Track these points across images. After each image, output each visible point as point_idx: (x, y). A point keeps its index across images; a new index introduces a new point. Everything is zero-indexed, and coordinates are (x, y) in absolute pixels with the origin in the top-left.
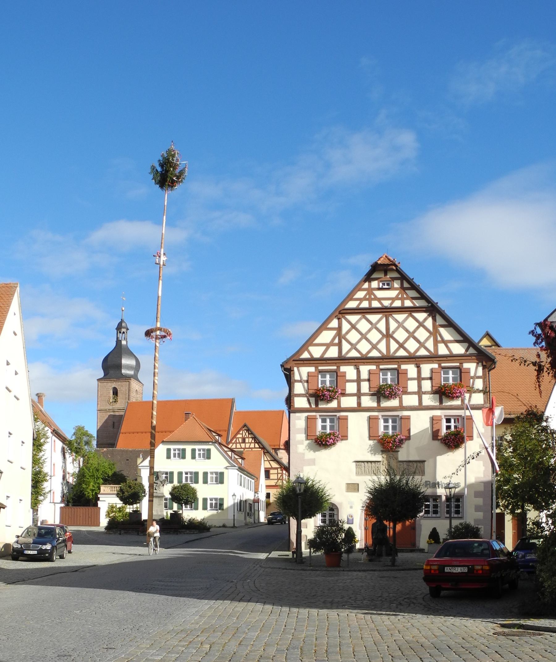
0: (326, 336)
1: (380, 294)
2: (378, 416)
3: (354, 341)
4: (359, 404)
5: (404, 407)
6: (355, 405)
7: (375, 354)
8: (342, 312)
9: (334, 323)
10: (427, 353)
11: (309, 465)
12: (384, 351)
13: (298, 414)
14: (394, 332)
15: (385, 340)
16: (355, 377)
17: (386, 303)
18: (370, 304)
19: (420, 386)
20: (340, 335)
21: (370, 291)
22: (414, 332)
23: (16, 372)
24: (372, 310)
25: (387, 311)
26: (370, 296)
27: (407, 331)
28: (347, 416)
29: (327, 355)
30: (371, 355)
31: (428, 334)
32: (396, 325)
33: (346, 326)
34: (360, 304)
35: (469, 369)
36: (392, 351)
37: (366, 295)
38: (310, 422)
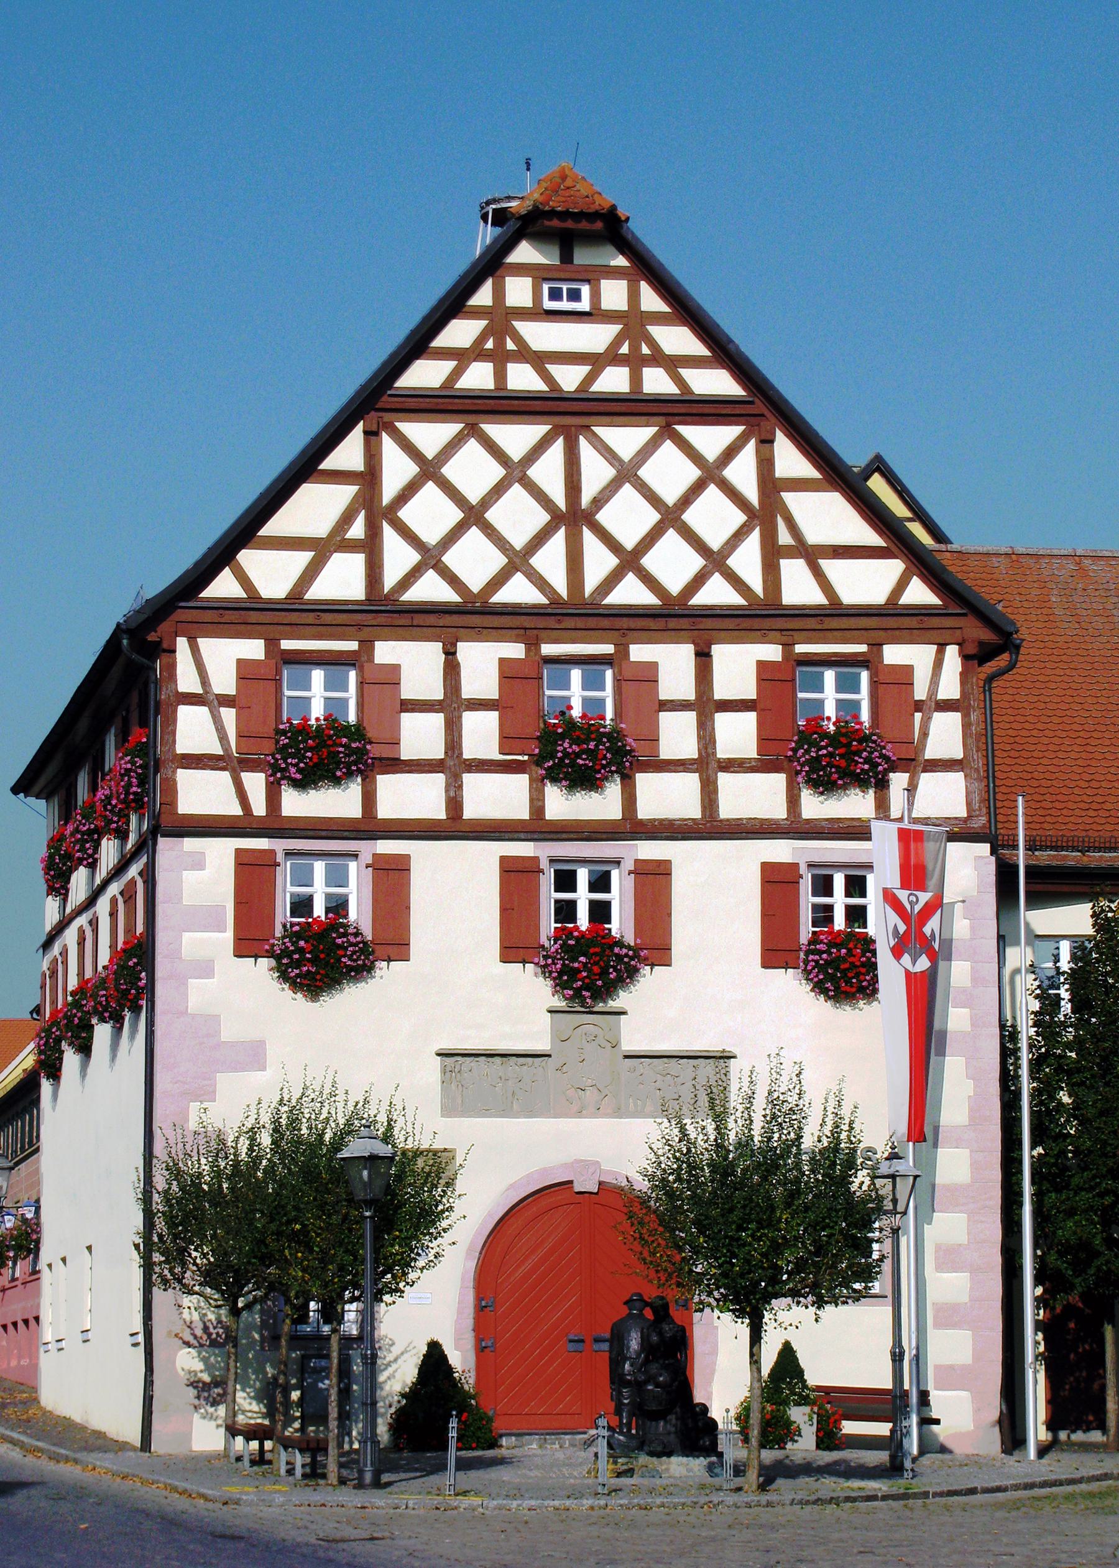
0: (314, 508)
1: (540, 335)
2: (536, 859)
3: (431, 536)
4: (454, 804)
5: (642, 823)
6: (437, 811)
7: (519, 591)
8: (376, 403)
9: (349, 454)
10: (735, 599)
11: (237, 1067)
12: (560, 583)
13: (190, 844)
14: (599, 502)
15: (561, 535)
16: (436, 691)
17: (569, 378)
18: (500, 375)
19: (706, 736)
20: (375, 509)
21: (501, 319)
22: (674, 509)
23: (90, 1252)
24: (506, 405)
25: (570, 414)
26: (500, 344)
27: (653, 499)
28: (407, 858)
29: (318, 591)
30: (502, 596)
31: (740, 518)
32: (535, 472)
33: (396, 469)
34: (590, 378)
35: (909, 670)
36: (591, 583)
37: (617, 342)
38: (253, 874)
